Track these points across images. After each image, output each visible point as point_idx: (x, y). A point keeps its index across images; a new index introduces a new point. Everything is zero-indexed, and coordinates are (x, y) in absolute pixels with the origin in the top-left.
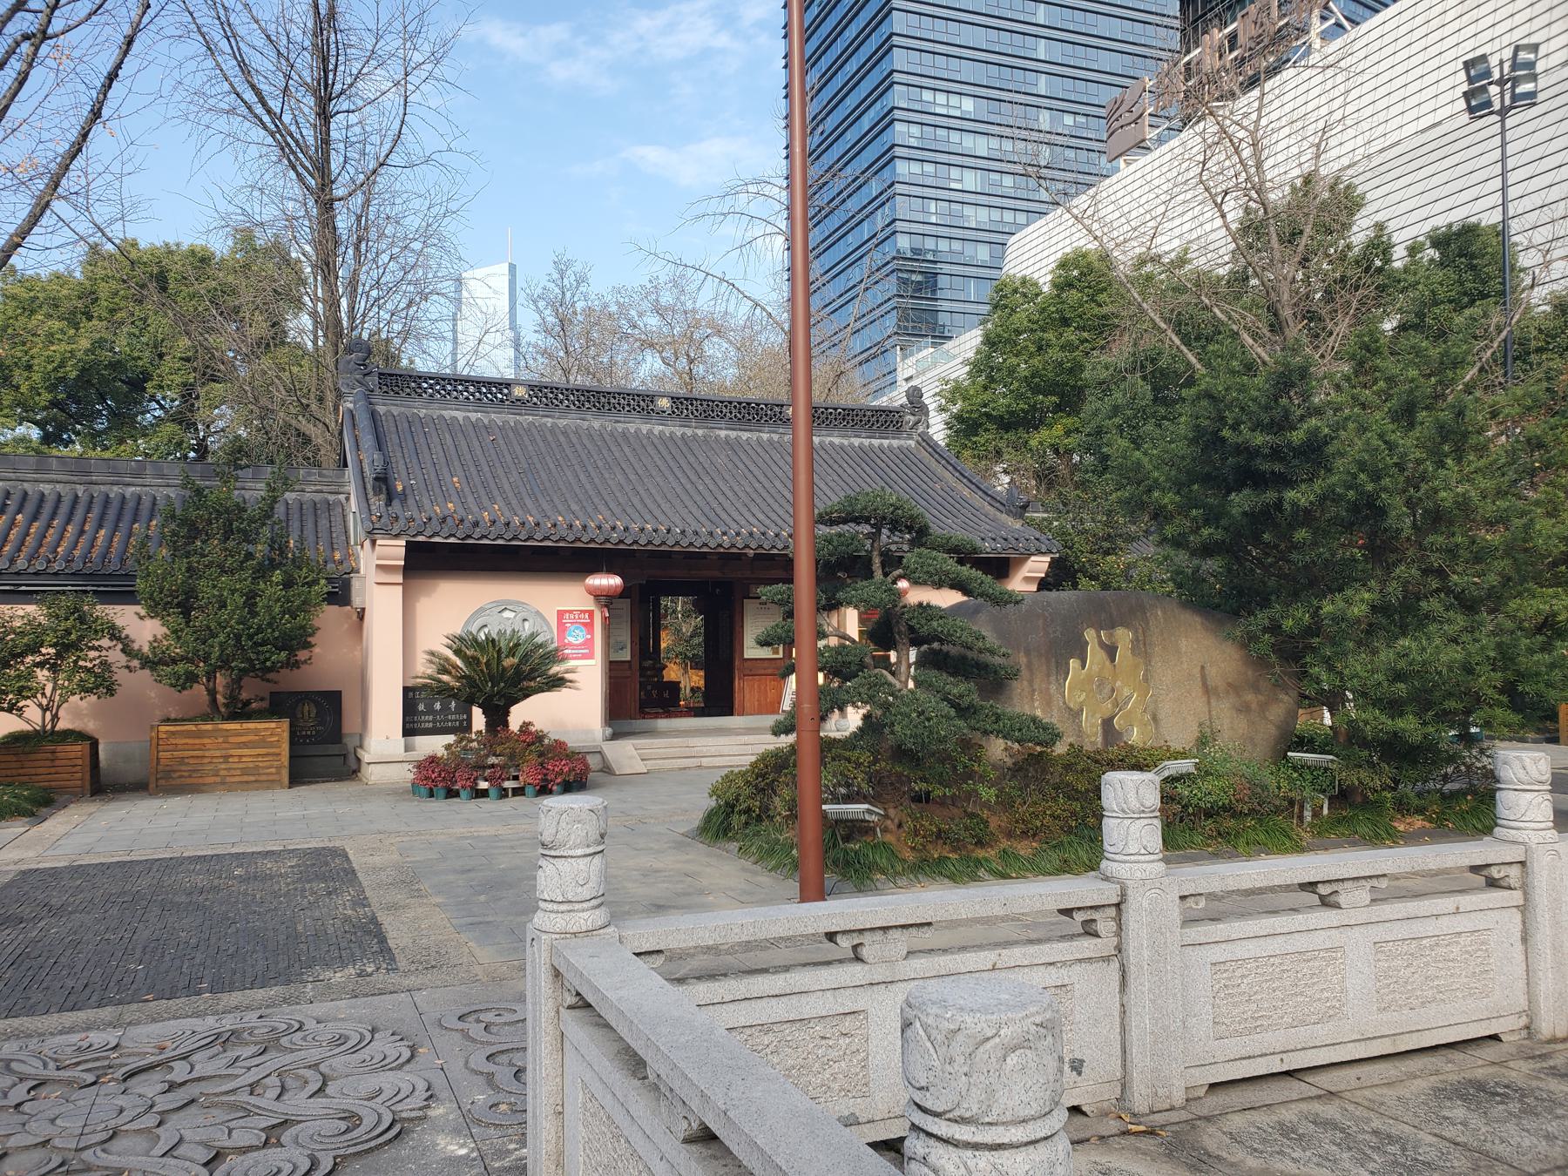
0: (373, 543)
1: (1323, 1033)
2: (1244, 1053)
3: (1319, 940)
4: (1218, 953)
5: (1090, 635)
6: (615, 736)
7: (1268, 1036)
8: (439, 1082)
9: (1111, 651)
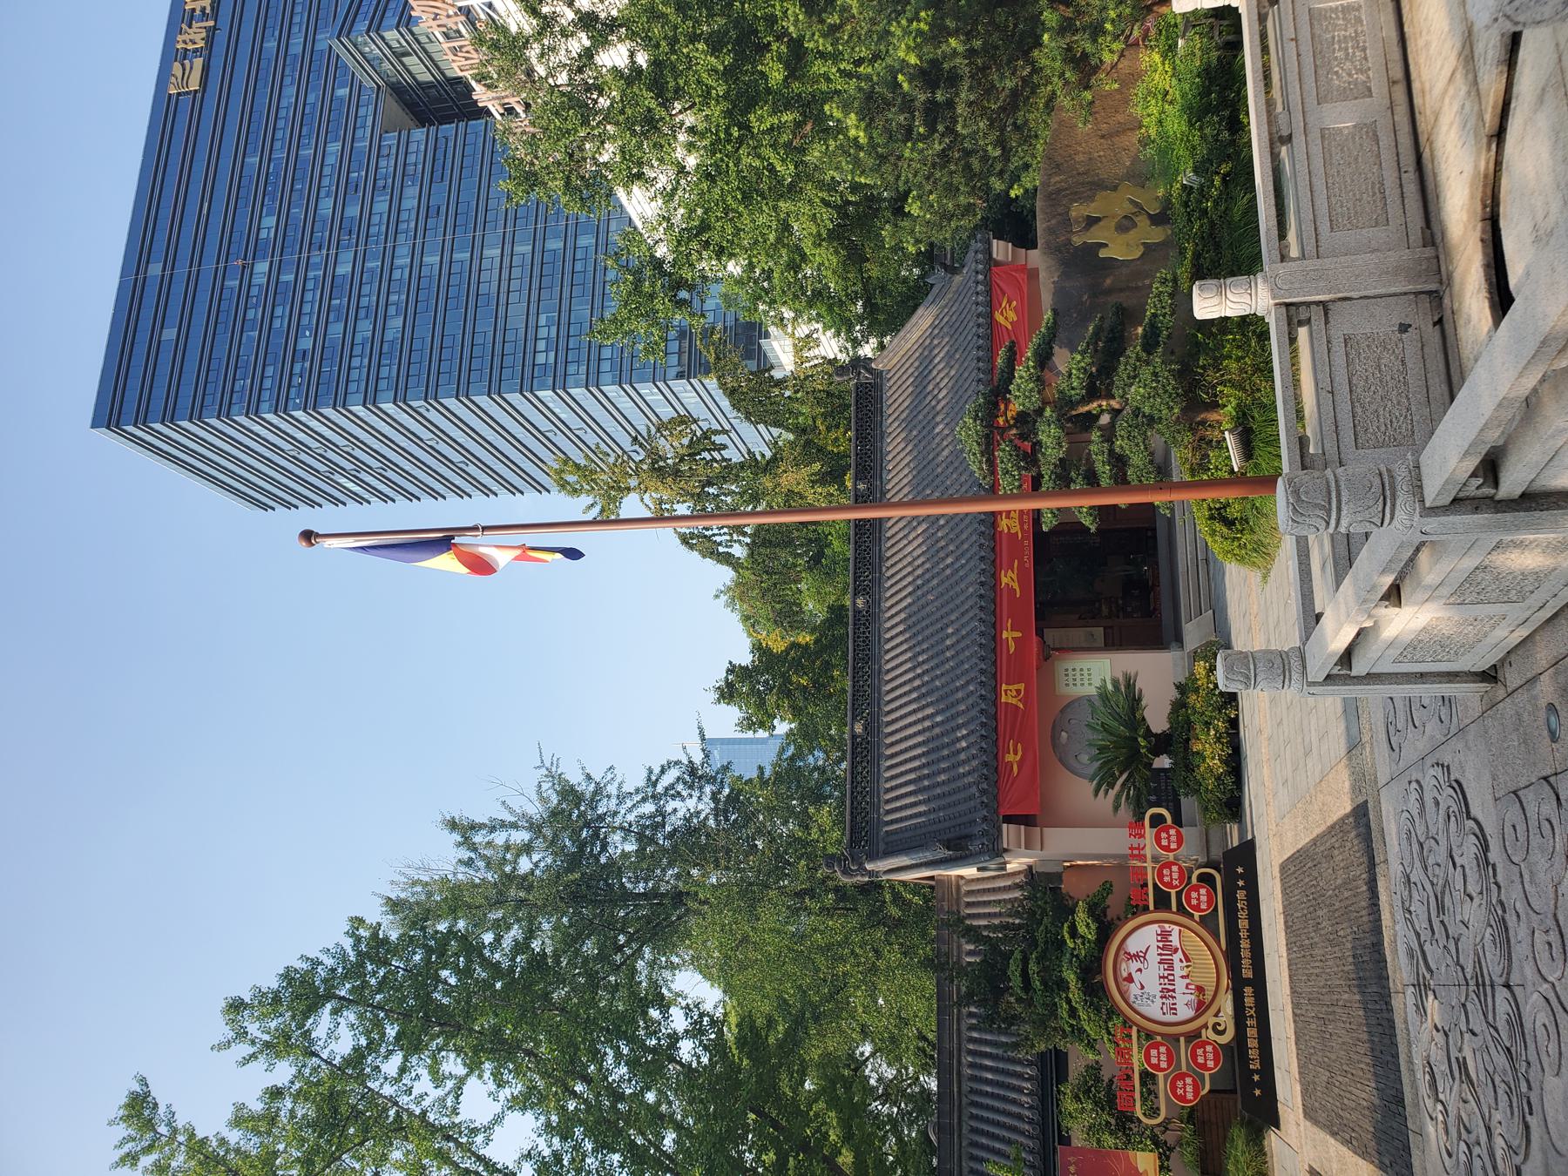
0: (1006, 850)
1: (1386, 140)
2: (1399, 202)
3: (1316, 150)
4: (1324, 227)
5: (1077, 240)
6: (1179, 639)
7: (1387, 184)
8: (1429, 761)
9: (1092, 221)
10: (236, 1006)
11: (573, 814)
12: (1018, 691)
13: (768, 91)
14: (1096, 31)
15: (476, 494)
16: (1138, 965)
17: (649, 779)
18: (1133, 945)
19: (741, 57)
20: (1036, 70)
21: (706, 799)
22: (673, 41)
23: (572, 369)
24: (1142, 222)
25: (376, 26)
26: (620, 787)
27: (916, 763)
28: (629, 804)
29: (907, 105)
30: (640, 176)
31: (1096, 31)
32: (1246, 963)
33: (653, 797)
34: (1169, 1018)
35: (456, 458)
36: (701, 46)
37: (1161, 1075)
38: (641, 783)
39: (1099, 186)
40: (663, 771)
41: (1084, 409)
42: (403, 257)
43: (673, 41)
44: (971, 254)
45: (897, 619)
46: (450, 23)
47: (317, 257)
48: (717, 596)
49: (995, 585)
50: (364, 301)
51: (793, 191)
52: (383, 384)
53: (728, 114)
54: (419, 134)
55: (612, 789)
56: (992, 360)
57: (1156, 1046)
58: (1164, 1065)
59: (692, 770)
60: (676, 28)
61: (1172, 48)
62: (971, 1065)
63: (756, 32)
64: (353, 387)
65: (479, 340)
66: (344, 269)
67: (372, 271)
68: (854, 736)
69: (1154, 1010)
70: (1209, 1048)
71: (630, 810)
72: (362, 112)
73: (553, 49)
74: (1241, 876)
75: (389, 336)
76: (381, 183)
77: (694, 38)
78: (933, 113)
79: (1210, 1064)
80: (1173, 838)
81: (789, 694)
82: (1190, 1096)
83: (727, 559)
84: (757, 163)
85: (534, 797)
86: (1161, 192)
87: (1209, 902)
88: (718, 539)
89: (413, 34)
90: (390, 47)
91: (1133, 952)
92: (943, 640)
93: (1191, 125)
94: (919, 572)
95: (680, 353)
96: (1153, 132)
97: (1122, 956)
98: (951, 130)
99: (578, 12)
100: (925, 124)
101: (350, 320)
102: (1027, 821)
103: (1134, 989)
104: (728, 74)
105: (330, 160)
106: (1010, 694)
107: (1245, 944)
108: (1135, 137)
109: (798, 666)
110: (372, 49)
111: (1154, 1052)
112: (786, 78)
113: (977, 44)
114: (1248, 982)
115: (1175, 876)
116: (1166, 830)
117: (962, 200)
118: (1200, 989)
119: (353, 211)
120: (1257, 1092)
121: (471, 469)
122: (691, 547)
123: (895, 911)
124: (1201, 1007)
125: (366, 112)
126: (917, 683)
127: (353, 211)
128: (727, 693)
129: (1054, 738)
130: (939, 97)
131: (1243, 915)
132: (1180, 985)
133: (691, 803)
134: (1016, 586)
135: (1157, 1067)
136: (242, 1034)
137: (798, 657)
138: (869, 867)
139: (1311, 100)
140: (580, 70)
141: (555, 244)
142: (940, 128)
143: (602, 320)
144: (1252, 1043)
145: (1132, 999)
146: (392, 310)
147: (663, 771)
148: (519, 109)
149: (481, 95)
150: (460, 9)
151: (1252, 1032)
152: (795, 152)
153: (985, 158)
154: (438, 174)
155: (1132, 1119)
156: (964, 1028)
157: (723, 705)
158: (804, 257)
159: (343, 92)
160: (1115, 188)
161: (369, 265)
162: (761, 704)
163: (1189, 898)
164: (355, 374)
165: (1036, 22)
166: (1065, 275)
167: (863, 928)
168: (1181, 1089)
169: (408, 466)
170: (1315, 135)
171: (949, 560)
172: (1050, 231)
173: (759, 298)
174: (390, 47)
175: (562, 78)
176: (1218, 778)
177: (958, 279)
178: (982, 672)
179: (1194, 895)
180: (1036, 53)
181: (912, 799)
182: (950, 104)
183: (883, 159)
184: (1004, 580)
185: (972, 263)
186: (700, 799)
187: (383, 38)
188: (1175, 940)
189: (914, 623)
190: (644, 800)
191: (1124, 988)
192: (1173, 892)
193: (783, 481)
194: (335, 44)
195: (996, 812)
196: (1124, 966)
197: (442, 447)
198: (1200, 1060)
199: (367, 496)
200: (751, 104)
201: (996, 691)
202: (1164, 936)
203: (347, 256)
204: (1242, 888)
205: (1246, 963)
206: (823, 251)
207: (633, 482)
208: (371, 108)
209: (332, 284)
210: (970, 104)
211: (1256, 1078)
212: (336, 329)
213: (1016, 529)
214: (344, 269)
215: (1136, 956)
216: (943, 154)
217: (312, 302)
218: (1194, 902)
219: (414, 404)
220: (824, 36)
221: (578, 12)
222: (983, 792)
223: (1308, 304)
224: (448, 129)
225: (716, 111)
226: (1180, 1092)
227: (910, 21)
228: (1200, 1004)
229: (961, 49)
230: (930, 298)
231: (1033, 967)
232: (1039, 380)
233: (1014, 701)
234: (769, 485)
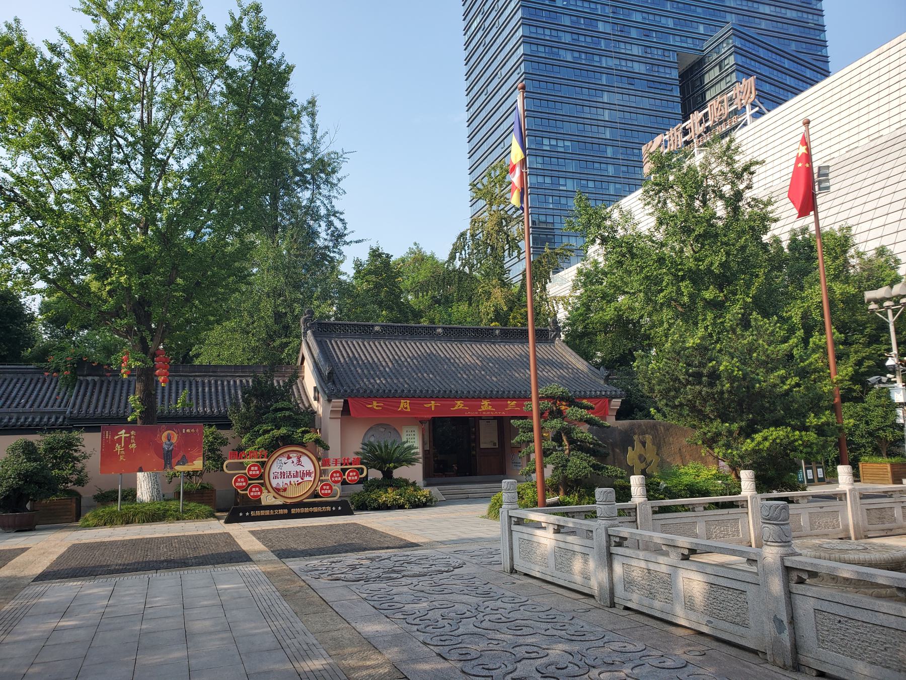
5: (636, 437)
9: (644, 444)
10: (257, 9)
13: (699, 290)
14: (728, 446)
15: (468, 99)
17: (337, 212)
18: (304, 459)
19: (717, 277)
20: (711, 420)
21: (326, 243)
22: (727, 244)
23: (540, 160)
24: (643, 466)
25: (738, 51)
26: (335, 197)
27: (364, 358)
28: (326, 202)
29: (702, 365)
30: (661, 223)
31: (728, 446)
32: (298, 510)
34: (272, 476)
35: (490, 88)
36: (724, 259)
38: (336, 209)
39: (659, 447)
40: (341, 220)
41: (564, 438)
42: (606, 61)
43: (727, 244)
44: (615, 389)
45: (432, 349)
46: (737, 101)
47: (608, 11)
48: (415, 244)
49: (456, 398)
50: (582, 38)
51: (648, 300)
52: (534, 48)
53: (690, 270)
54: (675, 74)
55: (334, 193)
56: (585, 398)
57: (259, 470)
59: (341, 236)
60: (733, 245)
61: (718, 479)
62: (210, 382)
63: (729, 285)
64: (533, 29)
65: (558, 105)
66: (601, 27)
67: (599, 43)
69: (275, 469)
71: (322, 202)
72: (690, 41)
73: (726, 179)
74: (337, 509)
75: (562, 52)
76: (649, 50)
77: (728, 254)
78: (698, 376)
79: (252, 494)
81: (375, 287)
82: (237, 484)
83: (452, 257)
84: (664, 284)
85: (330, 150)
86: (655, 474)
87: (324, 494)
88: (463, 252)
89: (731, 73)
90: (725, 59)
92: (426, 372)
93: (686, 485)
94: (457, 361)
95: (546, 222)
96: (682, 470)
98: (688, 382)
99: (743, 191)
100: (693, 373)
101: (573, 30)
102: (346, 410)
103: (284, 459)
104: (709, 271)
105: (663, 20)
106: (405, 405)
107: (307, 510)
108: (679, 463)
109: (391, 293)
110: (725, 48)
111: (256, 468)
112: (705, 299)
113: (726, 396)
114: (290, 511)
117: (657, 388)
118: (285, 490)
119: (634, 33)
122: (459, 238)
123: (278, 342)
124: (277, 490)
125: (689, 43)
126: (403, 359)
127: (634, 33)
129: (381, 425)
130: (704, 379)
131: (320, 509)
132: (287, 481)
133: (323, 235)
134: (456, 408)
136: (246, 13)
137: (395, 294)
138: (309, 332)
139: (706, 519)
140: (714, 191)
141: (610, 152)
142: (691, 379)
143: (588, 199)
144: (262, 513)
146: (576, 55)
147: (341, 220)
148: (687, 138)
149: (697, 116)
150: (745, 107)
151: (267, 512)
152: (668, 303)
153: (675, 397)
154: (652, 84)
156: (229, 378)
157: (369, 251)
158: (609, 302)
159: (701, 29)
160: (657, 454)
161: (603, 41)
162: (370, 272)
164: (540, 31)
165: (733, 421)
166: (621, 432)
167: (267, 326)
169: (486, 59)
170: (694, 520)
171: (465, 376)
172: (640, 426)
173: (588, 277)
174: (725, 59)
175: (711, 182)
176: (376, 500)
177: (602, 382)
178: (415, 391)
180: (719, 420)
181: (345, 355)
182: (700, 383)
183: (679, 354)
184: (459, 402)
185: (610, 389)
186: (326, 240)
187: (730, 55)
189: (431, 360)
190: (328, 210)
193: (496, 290)
194: (729, 26)
195: (350, 396)
197: (496, 81)
199: (469, 33)
200: (694, 282)
201: (407, 397)
202: (309, 474)
203: (608, 29)
205: (298, 510)
206: (613, 311)
207: (494, 208)
208: (691, 46)
209: (592, 19)
210: (700, 393)
212: (566, 21)
213: (483, 408)
214: (601, 27)
215: (299, 461)
216: (677, 379)
217: (583, 7)
219: (522, 66)
220: (731, 326)
221: (743, 191)
222: (358, 391)
223: (636, 516)
224: (677, 92)
225: (691, 264)
227: (738, 367)
229: (725, 388)
230: (593, 368)
231: (287, 413)
232: (581, 420)
233: (402, 406)
234: (494, 282)
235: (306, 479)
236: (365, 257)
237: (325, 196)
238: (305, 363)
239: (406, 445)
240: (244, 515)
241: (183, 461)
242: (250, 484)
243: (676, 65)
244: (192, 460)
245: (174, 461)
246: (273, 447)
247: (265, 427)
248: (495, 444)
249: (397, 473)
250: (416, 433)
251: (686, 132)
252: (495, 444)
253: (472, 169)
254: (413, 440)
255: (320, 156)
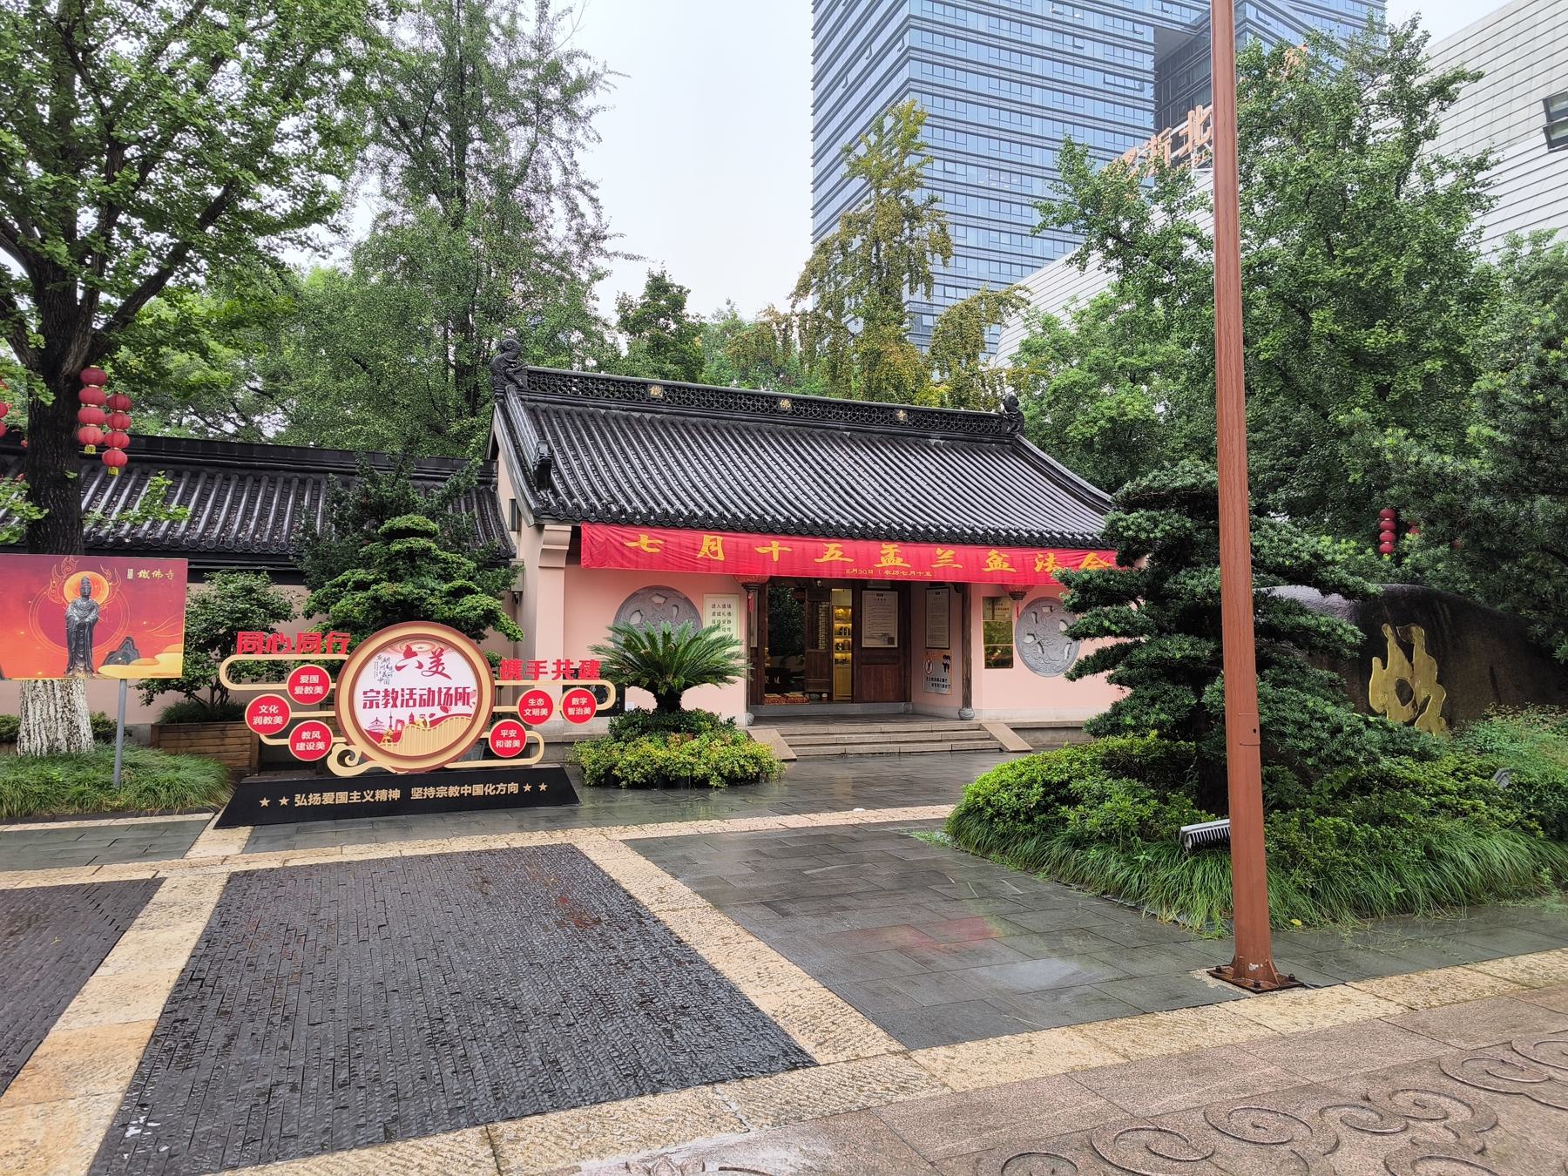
6: (757, 720)
11: (557, 91)
12: (715, 553)
16: (427, 663)
17: (585, 183)
18: (451, 660)
28: (562, 153)
33: (567, 185)
34: (359, 699)
37: (284, 686)
40: (592, 199)
54: (1148, 63)
58: (298, 690)
68: (645, 385)
69: (370, 680)
70: (321, 746)
74: (535, 788)
80: (580, 711)
82: (258, 720)
87: (504, 750)
91: (444, 658)
97: (438, 646)
102: (574, 554)
103: (396, 657)
111: (315, 679)
114: (406, 794)
115: (536, 712)
116: (591, 704)
120: (265, 802)
121: (839, 91)
128: (658, 286)
132: (402, 713)
134: (826, 558)
135: (295, 682)
144: (328, 798)
145: (383, 655)
147: (592, 199)
148: (1180, 152)
155: (226, 652)
157: (646, 279)
163: (508, 726)
168: (268, 708)
179: (513, 733)
188: (458, 708)
191: (398, 647)
192: (516, 709)
195: (586, 520)
196: (426, 647)
198: (305, 735)
204: (521, 789)
211: (284, 801)
213: (885, 562)
218: (504, 733)
226: (263, 709)
228: (379, 737)
231: (423, 542)
233: (705, 549)
235: (454, 709)
236: (637, 292)
237: (560, 140)
238: (501, 458)
239: (714, 636)
240: (274, 803)
241: (125, 654)
242: (296, 721)
243: (1151, 49)
244: (152, 652)
245: (98, 652)
246: (357, 629)
247: (361, 574)
248: (891, 640)
249: (692, 700)
250: (734, 610)
251: (1177, 142)
252: (891, 640)
253: (818, 209)
254: (727, 625)
255: (552, 56)
